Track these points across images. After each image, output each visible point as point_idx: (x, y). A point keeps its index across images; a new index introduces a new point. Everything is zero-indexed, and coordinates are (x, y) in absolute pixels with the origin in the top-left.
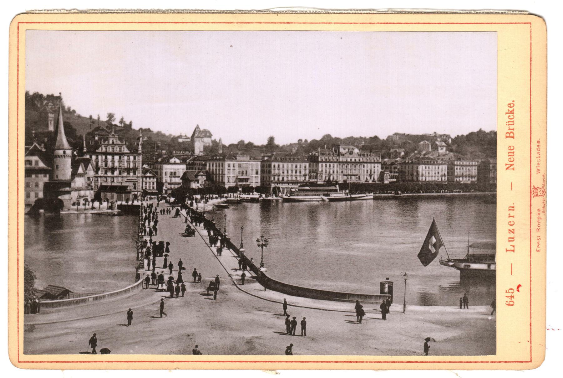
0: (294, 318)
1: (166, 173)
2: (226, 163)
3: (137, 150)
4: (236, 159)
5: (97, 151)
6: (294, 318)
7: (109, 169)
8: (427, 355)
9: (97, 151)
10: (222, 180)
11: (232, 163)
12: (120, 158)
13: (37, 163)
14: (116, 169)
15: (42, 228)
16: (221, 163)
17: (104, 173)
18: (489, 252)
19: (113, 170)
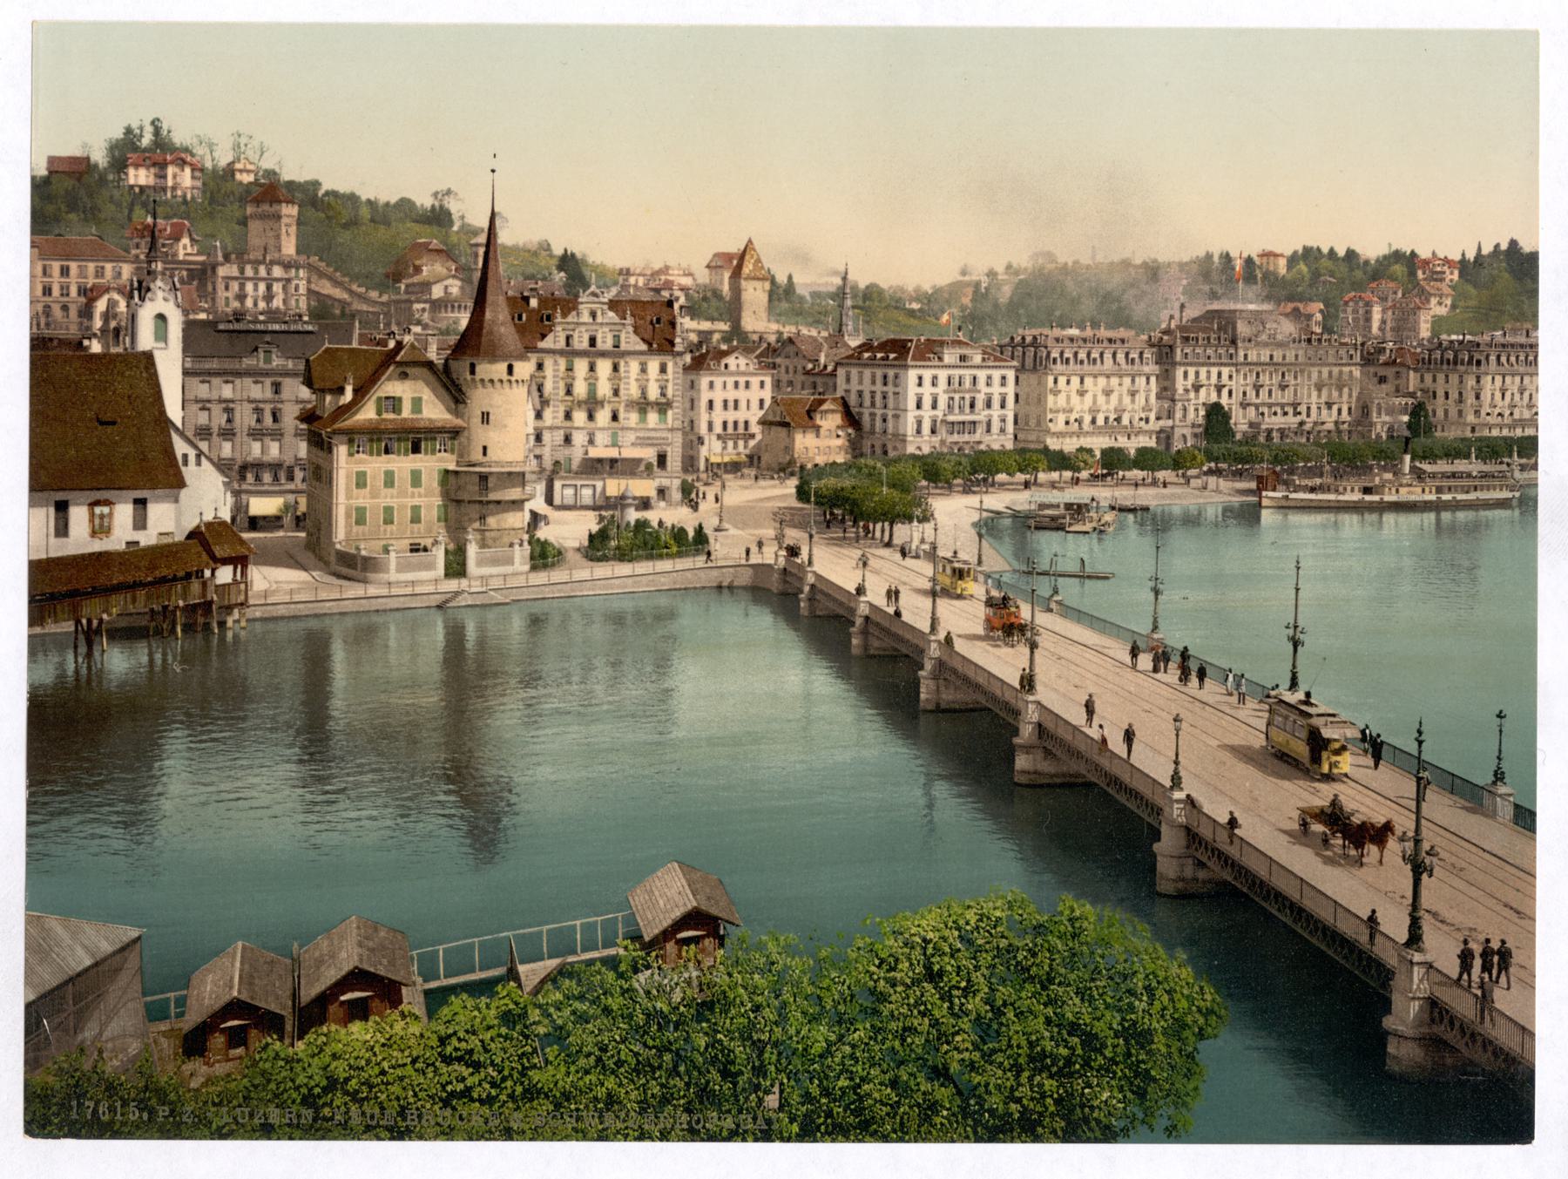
0: (1503, 942)
1: (711, 402)
2: (912, 375)
3: (672, 344)
4: (940, 359)
5: (541, 345)
6: (1503, 942)
7: (580, 403)
8: (1529, 447)
9: (541, 345)
10: (896, 427)
11: (927, 374)
12: (616, 368)
13: (417, 403)
14: (601, 403)
15: (490, 682)
16: (891, 373)
17: (561, 415)
18: (35, 829)
19: (592, 405)
